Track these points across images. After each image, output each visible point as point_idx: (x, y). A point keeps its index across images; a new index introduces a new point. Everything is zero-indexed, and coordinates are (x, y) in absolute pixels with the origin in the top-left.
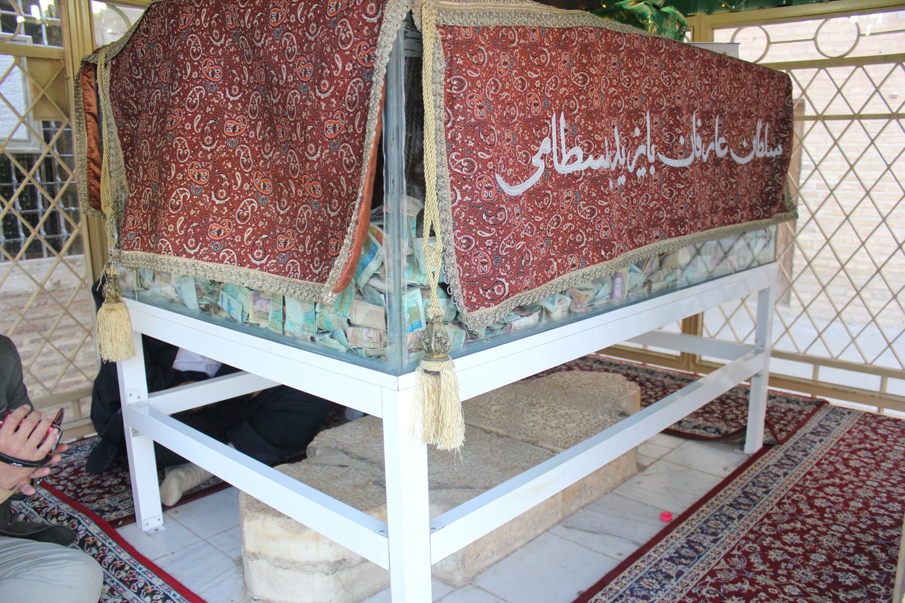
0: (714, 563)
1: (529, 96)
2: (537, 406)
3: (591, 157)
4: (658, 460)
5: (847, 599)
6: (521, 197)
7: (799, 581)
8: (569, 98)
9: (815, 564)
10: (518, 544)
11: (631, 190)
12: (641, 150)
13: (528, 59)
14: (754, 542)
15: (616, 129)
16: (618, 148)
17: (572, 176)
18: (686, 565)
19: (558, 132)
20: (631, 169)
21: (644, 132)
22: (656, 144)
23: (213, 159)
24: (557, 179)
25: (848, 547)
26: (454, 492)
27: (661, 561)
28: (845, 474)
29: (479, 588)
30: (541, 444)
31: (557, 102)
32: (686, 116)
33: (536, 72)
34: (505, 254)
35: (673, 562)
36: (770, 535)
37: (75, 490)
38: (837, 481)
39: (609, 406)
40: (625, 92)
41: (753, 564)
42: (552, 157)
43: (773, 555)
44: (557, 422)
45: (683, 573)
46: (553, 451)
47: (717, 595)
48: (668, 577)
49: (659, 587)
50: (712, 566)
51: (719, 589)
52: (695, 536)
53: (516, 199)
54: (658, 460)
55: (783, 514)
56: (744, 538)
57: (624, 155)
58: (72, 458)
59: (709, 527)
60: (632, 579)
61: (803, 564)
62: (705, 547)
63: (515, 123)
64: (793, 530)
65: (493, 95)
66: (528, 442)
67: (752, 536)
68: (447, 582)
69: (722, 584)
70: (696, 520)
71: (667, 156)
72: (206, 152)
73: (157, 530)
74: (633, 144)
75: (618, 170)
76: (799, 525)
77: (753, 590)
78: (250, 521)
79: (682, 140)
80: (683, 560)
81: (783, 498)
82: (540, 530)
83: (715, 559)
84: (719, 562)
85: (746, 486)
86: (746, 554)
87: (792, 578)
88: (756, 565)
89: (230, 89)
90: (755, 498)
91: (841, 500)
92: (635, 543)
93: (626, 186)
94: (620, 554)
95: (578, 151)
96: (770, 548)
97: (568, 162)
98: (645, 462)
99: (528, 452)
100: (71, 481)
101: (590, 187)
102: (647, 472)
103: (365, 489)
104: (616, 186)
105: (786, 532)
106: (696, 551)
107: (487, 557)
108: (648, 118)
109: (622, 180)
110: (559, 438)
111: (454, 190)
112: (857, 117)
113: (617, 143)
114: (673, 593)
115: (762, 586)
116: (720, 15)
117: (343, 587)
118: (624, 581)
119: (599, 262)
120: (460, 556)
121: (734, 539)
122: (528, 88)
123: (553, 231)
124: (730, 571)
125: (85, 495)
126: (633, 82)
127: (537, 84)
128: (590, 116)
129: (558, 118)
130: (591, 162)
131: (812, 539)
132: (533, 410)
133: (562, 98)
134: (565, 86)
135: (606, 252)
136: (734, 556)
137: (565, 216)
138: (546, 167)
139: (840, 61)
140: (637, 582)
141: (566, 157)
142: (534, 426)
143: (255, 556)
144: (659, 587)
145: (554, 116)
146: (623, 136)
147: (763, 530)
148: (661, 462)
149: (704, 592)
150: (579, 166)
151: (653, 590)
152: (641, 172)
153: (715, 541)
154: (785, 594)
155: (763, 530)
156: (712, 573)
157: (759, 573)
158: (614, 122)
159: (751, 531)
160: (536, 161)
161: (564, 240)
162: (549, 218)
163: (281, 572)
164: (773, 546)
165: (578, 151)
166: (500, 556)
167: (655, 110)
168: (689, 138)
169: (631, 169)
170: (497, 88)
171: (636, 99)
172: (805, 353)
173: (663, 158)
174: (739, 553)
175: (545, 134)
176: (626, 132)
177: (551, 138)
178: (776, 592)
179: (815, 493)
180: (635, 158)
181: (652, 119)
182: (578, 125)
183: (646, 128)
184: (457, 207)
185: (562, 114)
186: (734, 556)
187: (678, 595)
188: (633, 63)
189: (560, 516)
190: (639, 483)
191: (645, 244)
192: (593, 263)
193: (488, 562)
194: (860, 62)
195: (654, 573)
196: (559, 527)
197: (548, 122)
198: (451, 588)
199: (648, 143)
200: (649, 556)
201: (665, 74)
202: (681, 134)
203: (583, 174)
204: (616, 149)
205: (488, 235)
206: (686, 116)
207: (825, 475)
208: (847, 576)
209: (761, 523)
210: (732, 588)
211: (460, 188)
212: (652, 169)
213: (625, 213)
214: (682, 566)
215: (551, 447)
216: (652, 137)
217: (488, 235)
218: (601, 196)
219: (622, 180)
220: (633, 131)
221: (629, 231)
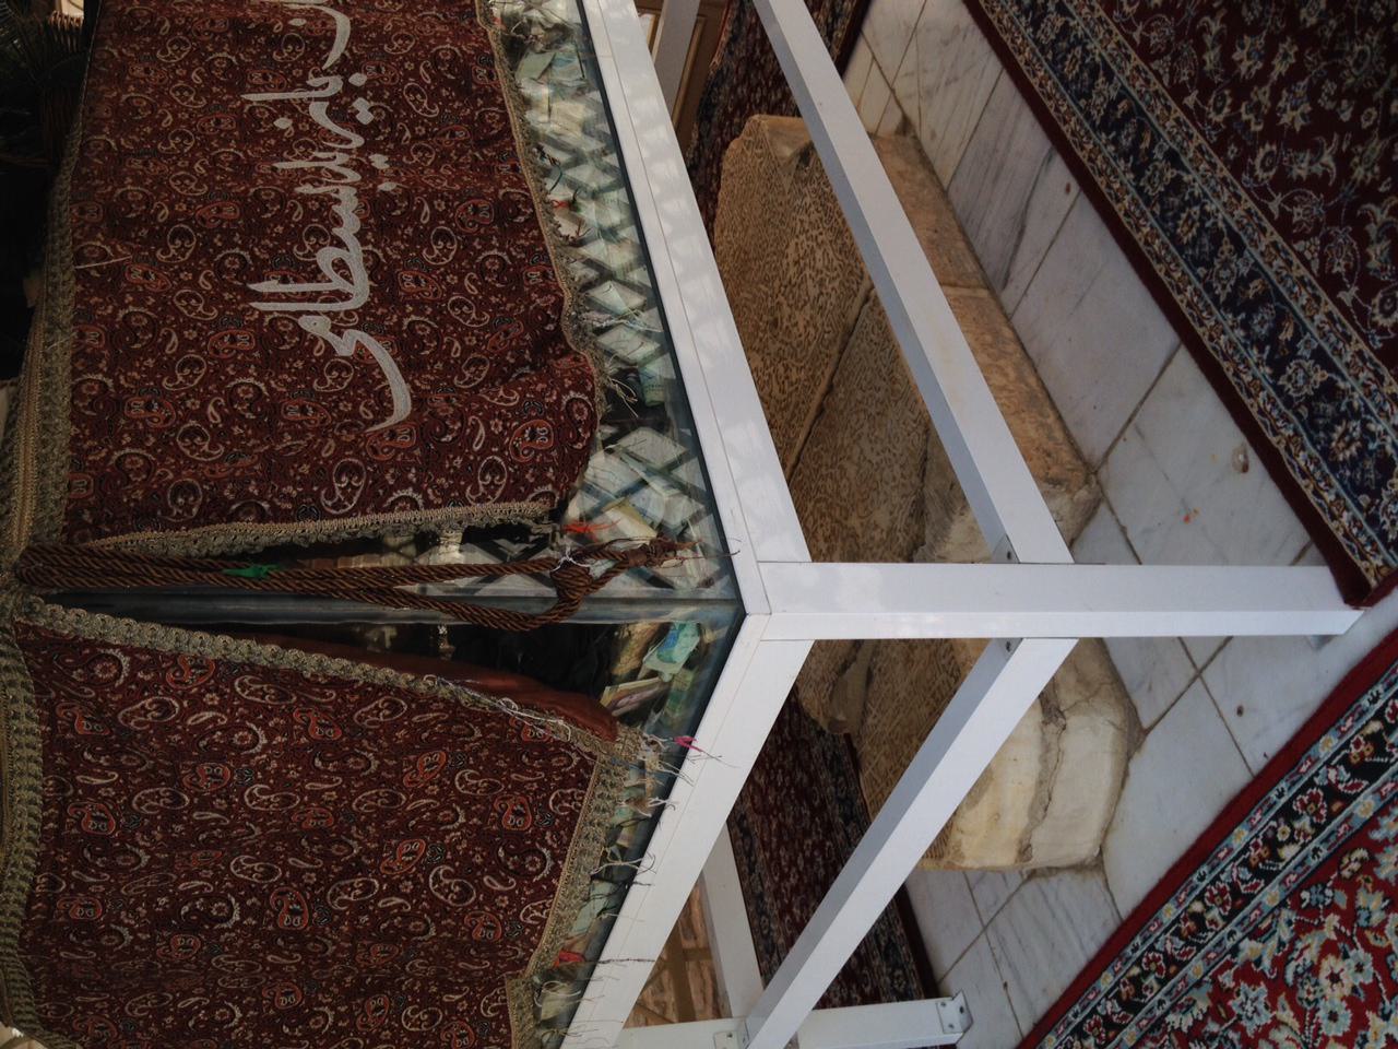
1: (217, 352)
2: (778, 314)
3: (336, 231)
4: (893, 91)
6: (415, 388)
8: (220, 269)
10: (1032, 381)
11: (397, 141)
12: (318, 112)
13: (140, 352)
15: (280, 165)
16: (316, 164)
17: (374, 269)
18: (1153, 143)
19: (288, 298)
20: (358, 141)
21: (284, 108)
22: (305, 77)
23: (347, 1002)
24: (381, 304)
26: (929, 491)
29: (1107, 454)
30: (850, 321)
31: (227, 296)
32: (249, 12)
33: (168, 337)
34: (437, 109)
35: (1145, 166)
39: (786, 182)
40: (204, 145)
42: (337, 314)
43: (1293, 117)
44: (810, 282)
45: (1320, 348)
46: (867, 299)
49: (1196, 209)
50: (1205, 146)
52: (1094, 112)
53: (419, 400)
54: (893, 91)
55: (1176, 55)
57: (330, 155)
59: (1194, 242)
61: (1327, 56)
62: (1120, 98)
63: (270, 390)
64: (1227, 43)
65: (213, 446)
66: (845, 344)
67: (1232, 151)
68: (1089, 513)
70: (1062, 104)
71: (330, 48)
72: (339, 1017)
73: (962, 1010)
74: (308, 133)
75: (359, 167)
78: (962, 857)
79: (298, 22)
80: (1145, 145)
82: (1007, 333)
83: (1147, 81)
84: (1156, 73)
85: (1088, 116)
86: (1282, 182)
88: (1318, 169)
89: (223, 1023)
90: (1123, 105)
92: (1049, 159)
93: (390, 153)
94: (1068, 189)
95: (326, 257)
96: (1271, 119)
97: (348, 278)
98: (894, 120)
99: (864, 345)
101: (395, 237)
102: (914, 116)
103: (934, 675)
104: (391, 173)
106: (1127, 116)
107: (1050, 437)
108: (255, 97)
109: (379, 161)
110: (842, 283)
111: (394, 503)
113: (305, 164)
117: (1087, 700)
119: (538, 228)
120: (1048, 487)
121: (1110, 32)
122: (200, 351)
123: (479, 314)
124: (1176, 55)
126: (183, 127)
127: (191, 334)
128: (254, 229)
129: (260, 297)
130: (348, 229)
132: (785, 324)
133: (222, 286)
134: (196, 276)
135: (519, 213)
136: (1145, 40)
137: (451, 289)
138: (357, 327)
141: (338, 283)
142: (815, 327)
143: (1024, 851)
144: (1079, 49)
145: (254, 304)
146: (291, 152)
148: (896, 86)
150: (354, 255)
151: (1083, 59)
152: (363, 110)
153: (1109, 76)
158: (265, 168)
160: (345, 346)
161: (496, 292)
162: (455, 323)
163: (1055, 808)
165: (326, 257)
166: (1049, 411)
167: (237, 80)
168: (294, 11)
169: (358, 141)
170: (187, 89)
171: (218, 122)
173: (334, 56)
175: (291, 327)
176: (284, 146)
177: (299, 314)
180: (336, 129)
181: (256, 89)
182: (272, 252)
183: (276, 102)
184: (426, 496)
185: (253, 287)
186: (1145, 40)
187: (1219, 175)
188: (144, 122)
189: (984, 293)
190: (933, 135)
191: (502, 106)
192: (540, 238)
193: (1059, 435)
197: (267, 319)
198: (1103, 508)
199: (305, 95)
200: (1261, 412)
201: (164, 52)
202: (285, 23)
203: (370, 247)
204: (318, 169)
205: (482, 431)
206: (249, 12)
211: (390, 490)
212: (358, 79)
213: (443, 157)
214: (1156, 150)
215: (858, 301)
216: (292, 88)
217: (482, 431)
218: (412, 216)
219: (379, 161)
220: (283, 131)
221: (479, 145)
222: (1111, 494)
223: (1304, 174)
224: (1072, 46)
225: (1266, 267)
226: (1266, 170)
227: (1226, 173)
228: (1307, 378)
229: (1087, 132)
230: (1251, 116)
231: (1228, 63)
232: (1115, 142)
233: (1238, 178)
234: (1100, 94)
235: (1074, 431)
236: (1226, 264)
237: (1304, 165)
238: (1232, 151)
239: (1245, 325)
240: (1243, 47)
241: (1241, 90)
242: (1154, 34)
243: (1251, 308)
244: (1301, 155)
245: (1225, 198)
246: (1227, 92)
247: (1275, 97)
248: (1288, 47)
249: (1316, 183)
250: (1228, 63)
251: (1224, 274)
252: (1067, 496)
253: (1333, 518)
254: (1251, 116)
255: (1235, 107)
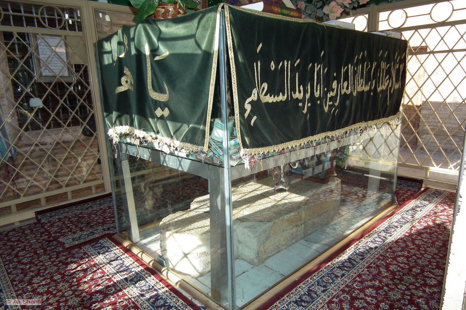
0: (360, 270)
5: (430, 292)
7: (398, 291)
9: (418, 267)
14: (382, 261)
18: (346, 270)
25: (432, 266)
27: (334, 268)
28: (384, 277)
36: (391, 258)
37: (103, 219)
38: (406, 253)
41: (408, 245)
43: (392, 268)
47: (361, 287)
48: (337, 277)
49: (331, 281)
50: (347, 283)
51: (362, 284)
56: (377, 258)
58: (102, 207)
60: (296, 294)
62: (357, 262)
64: (373, 287)
67: (347, 289)
69: (364, 281)
76: (406, 253)
77: (381, 286)
80: (303, 304)
81: (371, 263)
82: (294, 241)
86: (378, 266)
87: (403, 280)
88: (383, 273)
90: (355, 263)
91: (407, 267)
96: (356, 298)
100: (102, 216)
105: (399, 256)
112: (451, 51)
114: (338, 285)
115: (385, 284)
116: (382, 5)
118: (315, 278)
125: (108, 221)
131: (413, 261)
139: (443, 24)
140: (321, 278)
144: (331, 281)
147: (387, 255)
149: (354, 285)
153: (324, 291)
154: (399, 289)
155: (387, 255)
156: (360, 276)
157: (384, 277)
159: (381, 255)
164: (392, 263)
172: (199, 273)
174: (402, 241)
178: (394, 287)
179: (391, 261)
186: (333, 302)
189: (303, 236)
193: (270, 255)
194: (453, 24)
195: (330, 274)
196: (302, 241)
198: (252, 266)
200: (284, 299)
207: (400, 249)
208: (431, 280)
209: (386, 251)
210: (369, 283)
222: (256, 268)
223: (344, 306)
224: (332, 279)
225: (319, 298)
226: (343, 297)
227: (341, 288)
228: (338, 273)
229: (308, 285)
230: (357, 293)
231: (368, 287)
232: (376, 238)
233: (341, 291)
234: (357, 257)
235: (271, 258)
236: (319, 289)
237: (346, 306)
238: (347, 289)
239: (305, 294)
240: (372, 290)
241: (362, 290)
242: (373, 269)
243: (309, 295)
244: (348, 305)
245: (335, 288)
246: (361, 287)
247: (396, 265)
248: (375, 301)
249: (380, 272)
250: (368, 287)
251: (317, 289)
252: (255, 257)
253: (287, 296)
254: (357, 293)
255: (358, 289)
